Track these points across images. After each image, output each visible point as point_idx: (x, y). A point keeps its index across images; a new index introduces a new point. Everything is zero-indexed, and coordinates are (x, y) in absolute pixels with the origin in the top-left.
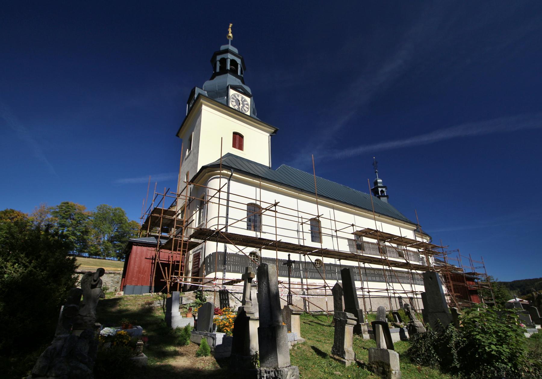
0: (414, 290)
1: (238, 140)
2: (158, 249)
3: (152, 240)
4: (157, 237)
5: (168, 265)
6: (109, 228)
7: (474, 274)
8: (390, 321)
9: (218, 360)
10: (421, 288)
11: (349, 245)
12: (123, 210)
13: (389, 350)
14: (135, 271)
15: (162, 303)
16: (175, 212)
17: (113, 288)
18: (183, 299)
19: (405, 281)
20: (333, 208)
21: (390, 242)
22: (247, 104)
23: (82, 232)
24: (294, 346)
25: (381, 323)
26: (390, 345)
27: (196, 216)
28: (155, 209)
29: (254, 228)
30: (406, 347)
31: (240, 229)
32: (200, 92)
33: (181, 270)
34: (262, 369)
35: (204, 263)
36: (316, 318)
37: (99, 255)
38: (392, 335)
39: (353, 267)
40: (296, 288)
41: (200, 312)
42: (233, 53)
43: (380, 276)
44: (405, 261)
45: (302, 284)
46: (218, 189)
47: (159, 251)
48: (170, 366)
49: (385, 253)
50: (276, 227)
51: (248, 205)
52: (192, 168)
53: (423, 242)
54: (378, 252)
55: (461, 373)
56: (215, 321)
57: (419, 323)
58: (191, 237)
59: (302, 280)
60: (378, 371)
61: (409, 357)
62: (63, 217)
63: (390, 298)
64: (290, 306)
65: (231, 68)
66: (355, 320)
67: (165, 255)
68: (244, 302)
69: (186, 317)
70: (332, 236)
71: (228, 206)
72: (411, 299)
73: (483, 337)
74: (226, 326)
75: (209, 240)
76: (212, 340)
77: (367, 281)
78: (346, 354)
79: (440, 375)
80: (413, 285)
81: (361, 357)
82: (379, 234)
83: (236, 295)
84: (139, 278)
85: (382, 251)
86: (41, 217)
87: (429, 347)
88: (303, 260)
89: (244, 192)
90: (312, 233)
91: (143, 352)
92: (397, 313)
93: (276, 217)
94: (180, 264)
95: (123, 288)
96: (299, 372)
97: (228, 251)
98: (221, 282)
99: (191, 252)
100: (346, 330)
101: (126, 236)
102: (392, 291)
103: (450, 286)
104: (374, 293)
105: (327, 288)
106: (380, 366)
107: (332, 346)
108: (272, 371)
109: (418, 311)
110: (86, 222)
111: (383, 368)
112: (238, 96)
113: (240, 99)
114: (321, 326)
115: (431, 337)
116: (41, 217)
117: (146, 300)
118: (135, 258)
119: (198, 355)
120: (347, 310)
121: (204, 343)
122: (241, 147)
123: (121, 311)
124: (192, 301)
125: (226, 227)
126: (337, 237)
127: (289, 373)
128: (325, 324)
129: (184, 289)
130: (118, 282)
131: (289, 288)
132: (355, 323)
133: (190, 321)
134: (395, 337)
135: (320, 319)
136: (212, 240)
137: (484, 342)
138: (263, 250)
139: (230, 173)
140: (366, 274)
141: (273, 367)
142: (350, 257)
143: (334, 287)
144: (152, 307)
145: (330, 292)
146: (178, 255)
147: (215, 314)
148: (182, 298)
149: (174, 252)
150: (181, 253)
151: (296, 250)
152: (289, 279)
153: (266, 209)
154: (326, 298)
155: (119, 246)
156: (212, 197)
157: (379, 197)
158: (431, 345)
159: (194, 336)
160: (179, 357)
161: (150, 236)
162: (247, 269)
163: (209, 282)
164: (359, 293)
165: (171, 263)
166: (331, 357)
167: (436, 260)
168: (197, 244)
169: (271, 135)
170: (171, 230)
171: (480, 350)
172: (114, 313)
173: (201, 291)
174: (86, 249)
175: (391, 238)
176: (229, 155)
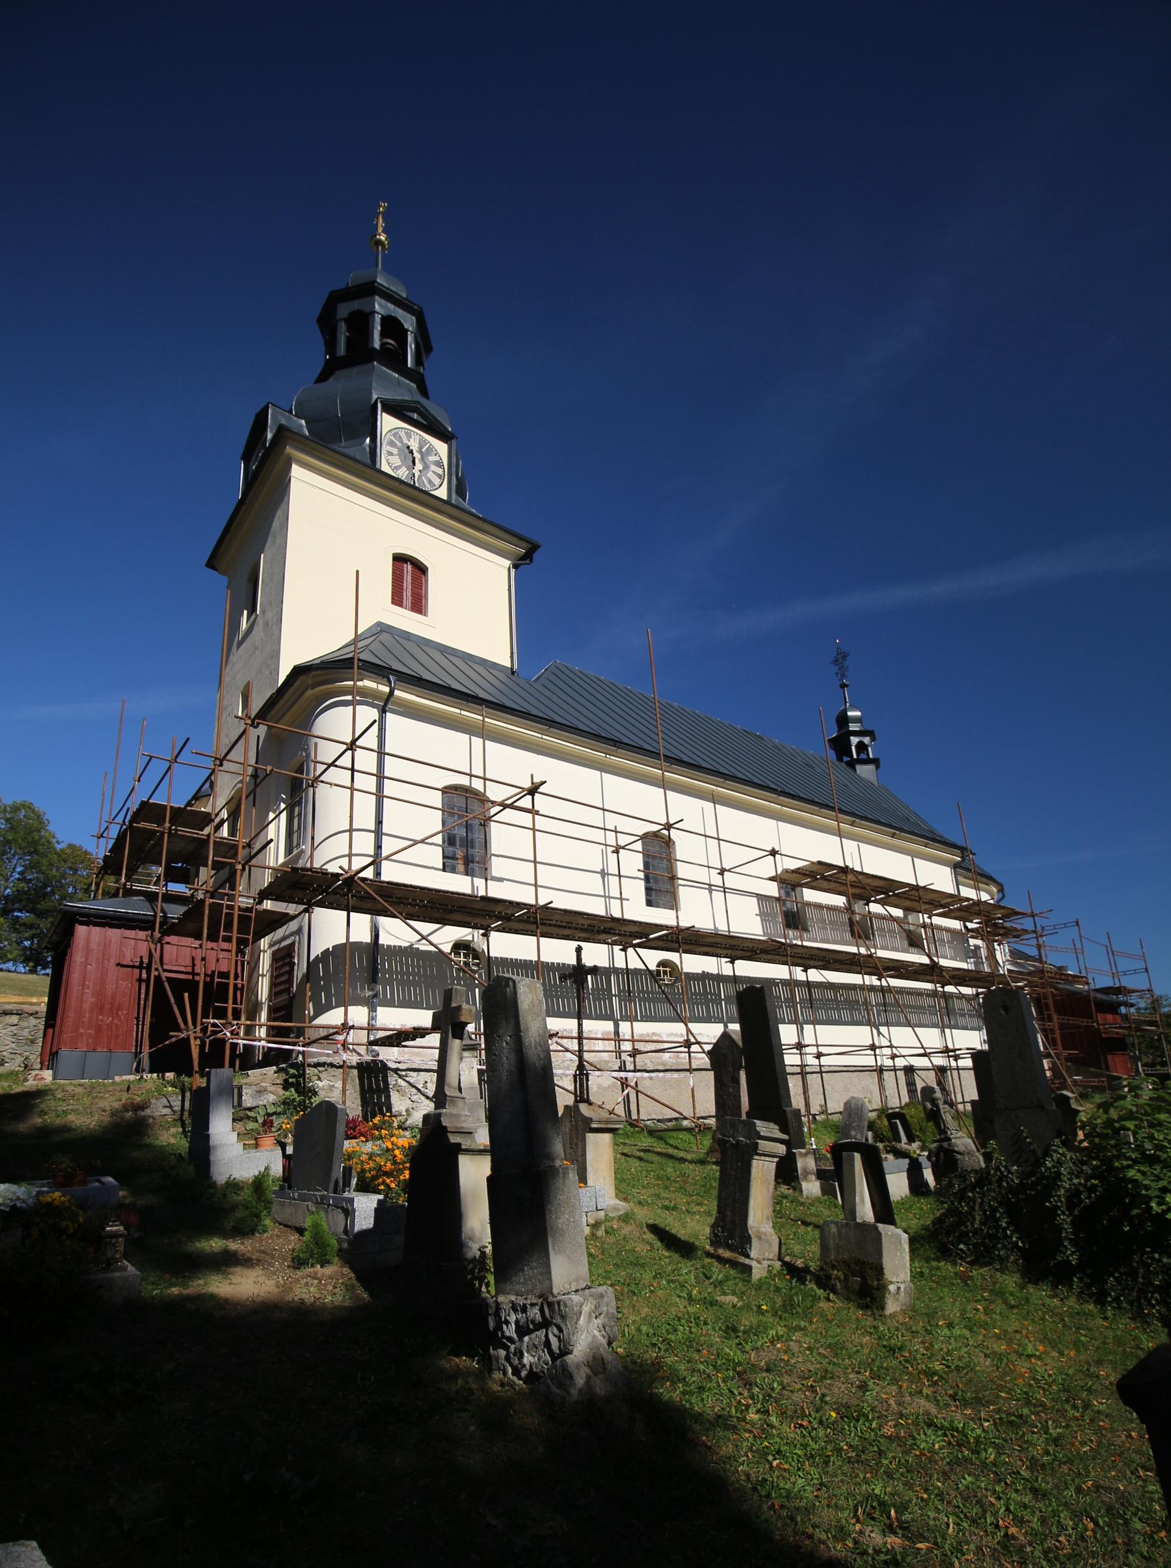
0: (951, 1046)
1: (409, 578)
2: (157, 934)
3: (137, 908)
4: (151, 897)
5: (191, 986)
7: (1118, 990)
8: (882, 1141)
9: (363, 1276)
10: (972, 1039)
11: (762, 914)
12: (40, 806)
13: (880, 1226)
14: (87, 1006)
15: (177, 1105)
16: (208, 814)
17: (19, 1060)
18: (244, 1091)
19: (925, 1018)
20: (714, 799)
21: (883, 903)
22: (439, 464)
24: (596, 1226)
25: (858, 1145)
26: (885, 1210)
27: (277, 830)
28: (144, 805)
29: (466, 864)
30: (926, 1212)
31: (422, 869)
32: (283, 422)
33: (235, 1002)
34: (501, 1299)
35: (307, 977)
36: (660, 1138)
38: (889, 1178)
39: (771, 982)
40: (599, 1052)
41: (300, 1132)
43: (852, 1005)
44: (925, 960)
45: (617, 1037)
46: (349, 740)
47: (160, 940)
48: (213, 1297)
49: (868, 938)
50: (535, 862)
51: (446, 790)
52: (260, 672)
53: (979, 903)
54: (848, 935)
55: (1081, 1279)
56: (350, 1157)
57: (963, 1140)
58: (264, 895)
59: (617, 1026)
60: (846, 1288)
61: (932, 1243)
63: (880, 1070)
64: (583, 1108)
65: (383, 345)
66: (781, 1141)
67: (180, 954)
68: (440, 1098)
69: (257, 1146)
70: (710, 887)
71: (380, 797)
72: (941, 1071)
73: (1144, 1174)
74: (386, 1174)
75: (321, 904)
76: (341, 1217)
77: (815, 1022)
78: (755, 1243)
79: (1022, 1287)
80: (947, 1031)
81: (797, 1249)
82: (851, 877)
83: (413, 1077)
84: (99, 1028)
85: (861, 930)
87: (995, 1210)
88: (620, 963)
89: (431, 751)
90: (647, 879)
91: (126, 1256)
92: (900, 1116)
93: (534, 830)
94: (232, 981)
95: (50, 1059)
96: (614, 1303)
97: (384, 940)
98: (363, 1036)
99: (264, 943)
100: (754, 1171)
101: (53, 893)
102: (888, 1051)
103: (1052, 1030)
104: (838, 1059)
105: (694, 1048)
106: (854, 1275)
107: (711, 1220)
108: (533, 1305)
109: (960, 1107)
111: (864, 1278)
112: (409, 437)
113: (414, 446)
114: (677, 1165)
115: (1000, 1181)
117: (125, 1097)
118: (86, 963)
119: (298, 1263)
120: (757, 1111)
121: (316, 1225)
122: (419, 605)
123: (45, 1132)
124: (272, 1098)
125: (376, 862)
126: (725, 890)
127: (586, 1309)
128: (689, 1157)
129: (246, 1060)
130: (33, 1042)
131: (581, 1051)
132: (781, 1149)
133: (269, 1161)
134: (898, 1184)
135: (671, 1141)
136: (331, 906)
137: (1147, 1188)
138: (494, 935)
139: (387, 689)
140: (811, 1003)
141: (537, 1292)
142: (763, 951)
143: (716, 1045)
144: (145, 1118)
145: (702, 1060)
146: (222, 955)
147: (348, 1137)
148: (240, 1089)
149: (210, 945)
150: (233, 946)
151: (600, 932)
152: (580, 1025)
153: (504, 806)
154: (691, 1079)
155: (31, 926)
156: (329, 766)
157: (852, 764)
158: (1000, 1204)
159: (283, 1205)
160: (238, 1270)
161: (129, 893)
162: (448, 995)
163: (326, 1038)
164: (791, 1059)
165: (201, 979)
166: (708, 1255)
167: (1015, 955)
168: (282, 919)
169: (516, 566)
170: (197, 875)
171: (1135, 1212)
173: (301, 1067)
175: (886, 889)
176: (381, 629)
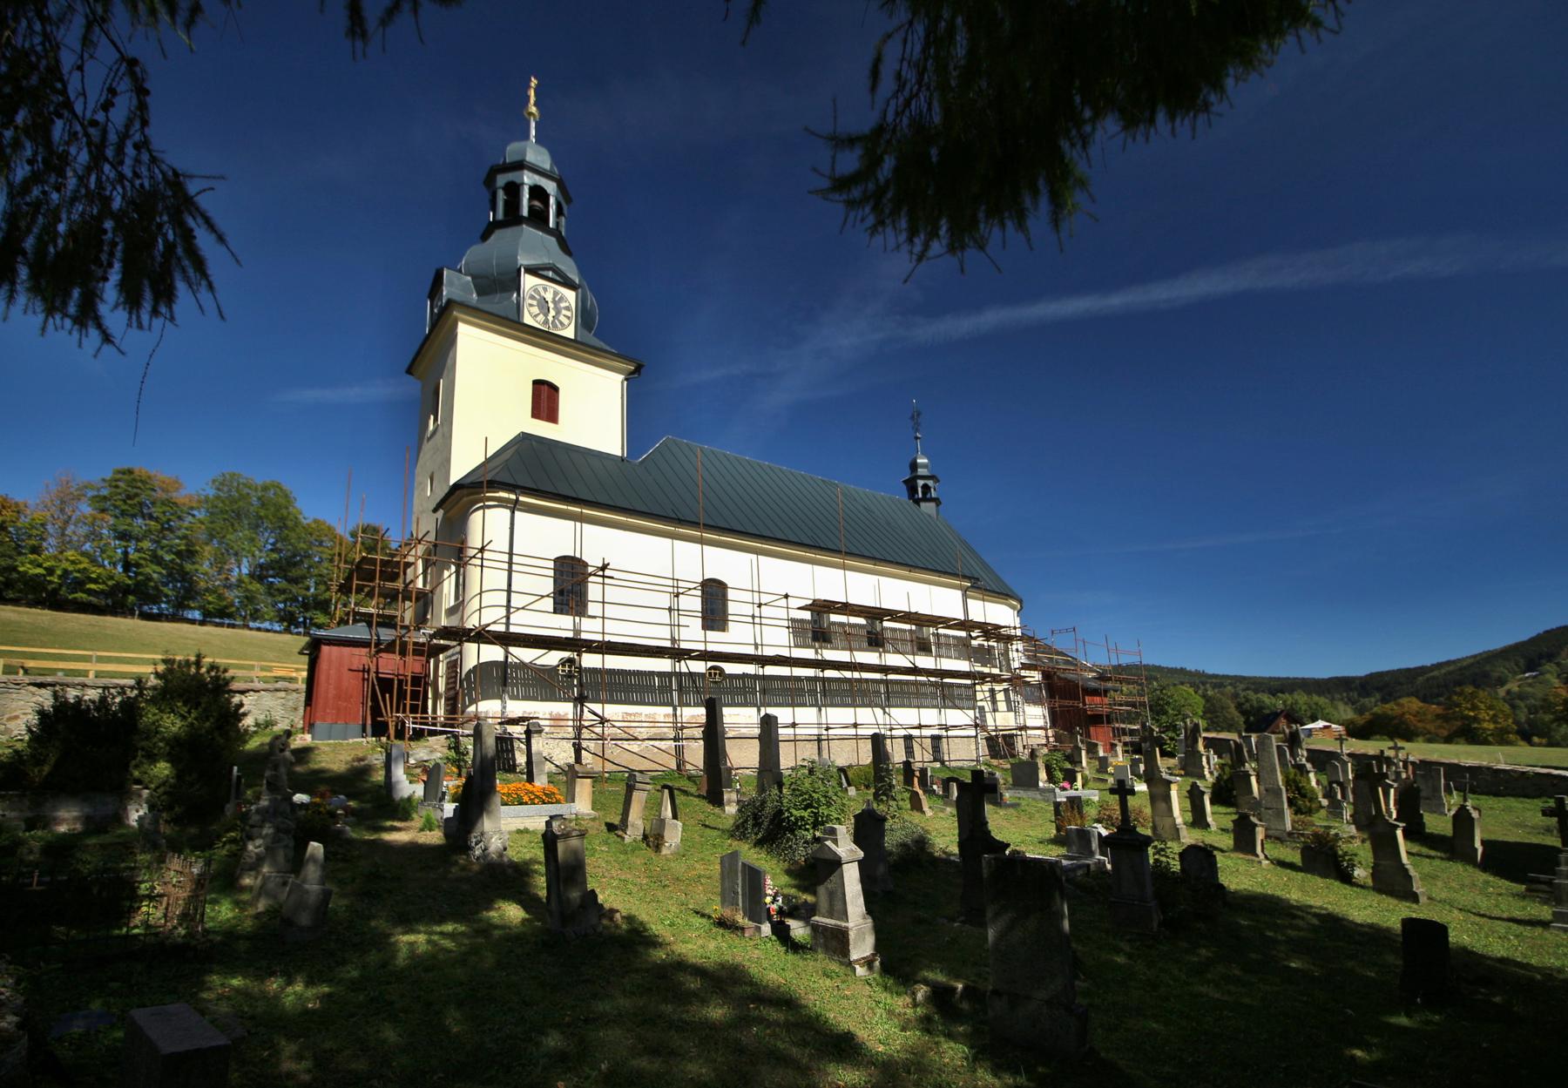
1: (545, 399)
6: (252, 540)
12: (287, 487)
22: (568, 308)
23: (179, 554)
37: (230, 616)
42: (535, 170)
62: (123, 513)
86: (62, 511)
89: (546, 535)
110: (186, 524)
112: (545, 290)
113: (549, 297)
116: (62, 511)
119: (422, 830)
155: (282, 592)
157: (917, 502)
172: (301, 774)
174: (193, 598)
176: (524, 438)
